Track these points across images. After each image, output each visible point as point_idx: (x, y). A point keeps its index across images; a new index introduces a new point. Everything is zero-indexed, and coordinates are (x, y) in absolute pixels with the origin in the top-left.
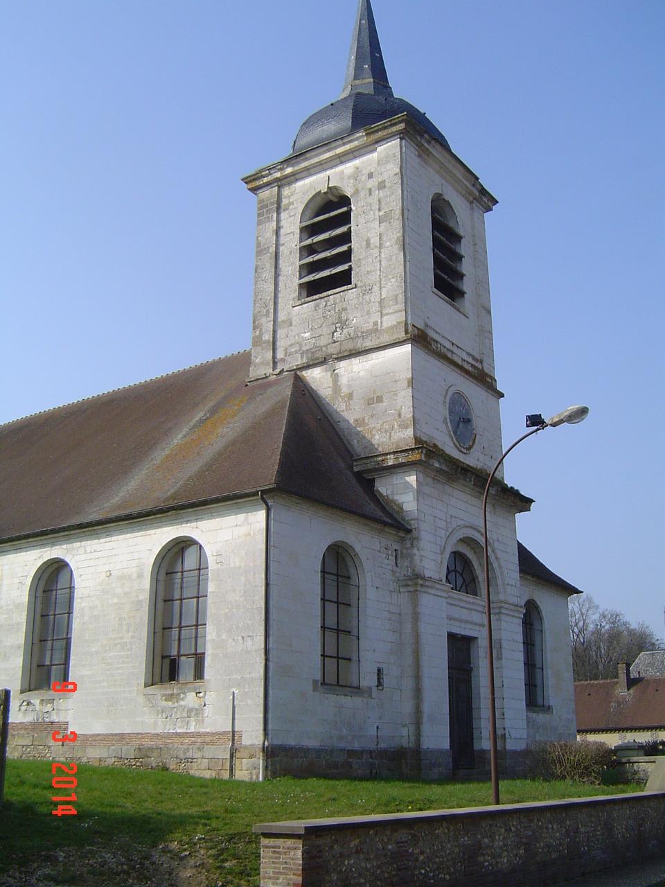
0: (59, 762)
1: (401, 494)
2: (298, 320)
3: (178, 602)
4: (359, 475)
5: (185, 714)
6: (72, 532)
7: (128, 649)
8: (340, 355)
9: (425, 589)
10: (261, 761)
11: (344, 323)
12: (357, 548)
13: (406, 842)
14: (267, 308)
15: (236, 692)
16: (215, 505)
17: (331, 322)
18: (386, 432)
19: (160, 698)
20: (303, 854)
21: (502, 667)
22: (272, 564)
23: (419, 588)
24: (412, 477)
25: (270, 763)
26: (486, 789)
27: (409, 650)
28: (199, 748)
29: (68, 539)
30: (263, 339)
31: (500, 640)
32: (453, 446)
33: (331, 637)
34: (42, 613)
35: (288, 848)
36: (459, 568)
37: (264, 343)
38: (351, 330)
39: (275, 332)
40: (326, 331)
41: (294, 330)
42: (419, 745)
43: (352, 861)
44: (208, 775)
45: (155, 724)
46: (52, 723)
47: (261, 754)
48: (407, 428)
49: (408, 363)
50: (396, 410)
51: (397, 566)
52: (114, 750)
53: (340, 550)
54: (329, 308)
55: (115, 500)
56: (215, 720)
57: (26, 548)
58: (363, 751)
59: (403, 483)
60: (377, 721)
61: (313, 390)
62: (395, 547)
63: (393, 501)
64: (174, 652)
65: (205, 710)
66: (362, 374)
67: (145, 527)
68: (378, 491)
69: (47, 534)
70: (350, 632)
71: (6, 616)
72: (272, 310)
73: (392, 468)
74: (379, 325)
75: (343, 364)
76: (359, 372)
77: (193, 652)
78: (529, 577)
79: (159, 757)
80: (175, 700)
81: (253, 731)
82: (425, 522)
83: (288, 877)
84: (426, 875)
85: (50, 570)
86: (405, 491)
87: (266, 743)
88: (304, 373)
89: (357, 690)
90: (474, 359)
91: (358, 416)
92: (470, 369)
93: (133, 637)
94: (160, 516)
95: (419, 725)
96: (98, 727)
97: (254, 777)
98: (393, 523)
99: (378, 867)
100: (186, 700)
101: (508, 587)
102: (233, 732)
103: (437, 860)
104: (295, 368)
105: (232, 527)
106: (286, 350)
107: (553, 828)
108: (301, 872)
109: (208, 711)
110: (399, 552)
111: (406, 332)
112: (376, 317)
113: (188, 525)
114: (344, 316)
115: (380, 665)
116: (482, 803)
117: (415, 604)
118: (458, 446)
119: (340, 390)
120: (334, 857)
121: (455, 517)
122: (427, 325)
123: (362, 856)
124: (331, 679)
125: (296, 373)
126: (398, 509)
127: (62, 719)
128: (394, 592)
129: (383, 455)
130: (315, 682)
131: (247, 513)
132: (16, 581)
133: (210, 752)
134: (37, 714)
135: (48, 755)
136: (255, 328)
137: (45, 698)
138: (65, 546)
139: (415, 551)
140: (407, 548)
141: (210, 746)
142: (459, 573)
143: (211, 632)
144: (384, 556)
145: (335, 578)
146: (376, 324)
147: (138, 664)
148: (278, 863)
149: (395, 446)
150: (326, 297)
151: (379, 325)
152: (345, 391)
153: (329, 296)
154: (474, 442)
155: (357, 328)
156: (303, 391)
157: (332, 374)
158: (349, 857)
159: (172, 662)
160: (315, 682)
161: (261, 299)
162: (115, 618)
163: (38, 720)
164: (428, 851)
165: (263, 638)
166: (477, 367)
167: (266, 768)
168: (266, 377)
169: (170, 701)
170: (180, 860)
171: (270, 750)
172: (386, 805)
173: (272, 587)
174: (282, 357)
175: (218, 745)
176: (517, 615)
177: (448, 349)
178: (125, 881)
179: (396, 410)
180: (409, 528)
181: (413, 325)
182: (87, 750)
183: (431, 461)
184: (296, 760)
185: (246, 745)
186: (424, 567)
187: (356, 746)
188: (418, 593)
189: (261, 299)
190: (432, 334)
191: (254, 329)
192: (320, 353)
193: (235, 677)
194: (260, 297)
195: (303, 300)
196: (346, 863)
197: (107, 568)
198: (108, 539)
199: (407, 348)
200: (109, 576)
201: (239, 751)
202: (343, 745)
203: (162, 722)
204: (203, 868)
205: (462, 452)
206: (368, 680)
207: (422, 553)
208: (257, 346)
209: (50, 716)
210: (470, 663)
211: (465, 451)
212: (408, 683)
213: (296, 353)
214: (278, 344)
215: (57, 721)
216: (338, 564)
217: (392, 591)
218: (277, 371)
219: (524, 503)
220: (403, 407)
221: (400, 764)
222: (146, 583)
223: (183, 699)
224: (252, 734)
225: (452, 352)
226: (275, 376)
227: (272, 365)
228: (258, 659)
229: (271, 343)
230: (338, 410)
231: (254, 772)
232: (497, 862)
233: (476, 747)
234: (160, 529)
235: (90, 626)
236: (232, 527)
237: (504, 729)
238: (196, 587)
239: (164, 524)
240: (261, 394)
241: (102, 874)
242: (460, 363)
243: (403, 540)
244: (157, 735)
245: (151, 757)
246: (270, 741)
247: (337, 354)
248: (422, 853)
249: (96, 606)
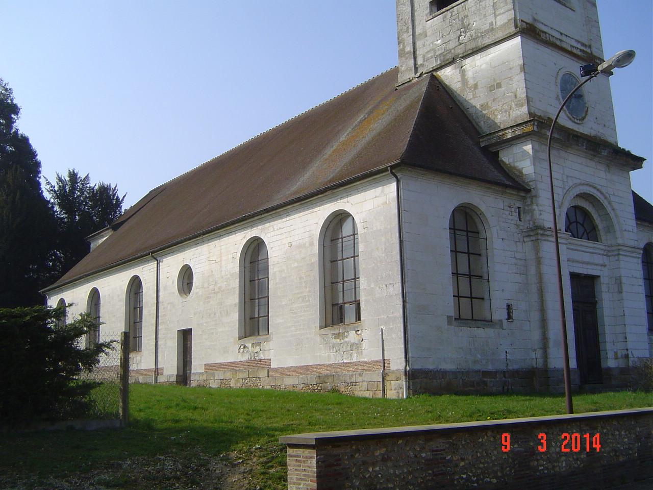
0: (267, 390)
1: (520, 161)
2: (431, 31)
3: (341, 261)
4: (485, 150)
5: (349, 348)
6: (263, 216)
7: (307, 301)
8: (465, 54)
9: (546, 238)
10: (404, 383)
11: (466, 28)
12: (483, 208)
13: (444, 450)
14: (407, 26)
15: (384, 329)
16: (358, 183)
17: (456, 29)
18: (506, 111)
19: (331, 336)
20: (317, 463)
21: (623, 300)
22: (404, 225)
23: (539, 237)
24: (528, 146)
25: (411, 384)
26: (563, 402)
27: (534, 288)
28: (360, 374)
29: (262, 221)
30: (406, 51)
31: (620, 277)
32: (567, 118)
33: (464, 282)
34: (250, 278)
35: (306, 457)
36: (580, 219)
37: (407, 53)
38: (473, 32)
39: (414, 44)
40: (453, 36)
41: (429, 40)
42: (547, 365)
43: (378, 468)
44: (368, 394)
45: (329, 356)
46: (260, 360)
47: (404, 377)
48: (522, 106)
49: (519, 52)
50: (513, 92)
51: (520, 221)
52: (302, 378)
53: (468, 211)
54: (454, 17)
55: (294, 188)
56: (370, 352)
57: (235, 232)
58: (497, 372)
59: (522, 152)
60: (512, 347)
61: (446, 85)
62: (518, 204)
63: (515, 168)
64: (341, 301)
65: (363, 344)
66: (484, 66)
67: (312, 206)
68: (503, 162)
69: (246, 219)
70: (482, 277)
71: (225, 283)
72: (411, 27)
73: (512, 140)
74: (494, 25)
75: (468, 61)
76: (481, 66)
77: (354, 300)
78: (647, 224)
79: (332, 382)
80: (341, 337)
81: (397, 359)
82: (542, 182)
83: (307, 483)
84: (468, 479)
85: (253, 246)
86: (524, 158)
87: (408, 368)
88: (438, 73)
89: (489, 323)
90: (583, 44)
91: (482, 102)
92: (580, 53)
93: (309, 291)
94: (320, 196)
95: (546, 349)
96: (290, 362)
97: (400, 395)
98: (514, 185)
99: (410, 473)
100: (349, 337)
101: (625, 233)
102: (384, 360)
103: (481, 465)
104: (431, 70)
105: (373, 199)
106: (424, 57)
107: (620, 435)
108: (316, 479)
109: (365, 345)
110: (522, 209)
111: (516, 27)
112: (491, 19)
113: (342, 201)
114: (466, 23)
115: (509, 302)
116: (559, 413)
117: (537, 250)
118: (571, 117)
119: (467, 83)
120: (355, 465)
121: (571, 177)
122: (535, 20)
123: (389, 464)
124: (466, 313)
125: (432, 74)
126: (518, 174)
127: (267, 357)
128: (519, 241)
129: (502, 130)
130: (449, 317)
131: (383, 186)
132: (231, 256)
133: (368, 376)
134: (250, 354)
135: (259, 384)
136: (399, 43)
137: (254, 342)
138: (259, 227)
139: (535, 207)
140: (528, 205)
141: (368, 372)
142: (580, 224)
143: (363, 283)
144: (507, 213)
145: (465, 233)
146: (491, 24)
147: (314, 312)
148: (299, 471)
149: (513, 122)
150: (450, 9)
151: (494, 25)
152: (471, 82)
153: (453, 7)
154: (586, 114)
155: (477, 30)
156: (438, 87)
157: (460, 71)
158: (374, 465)
159: (338, 310)
160: (449, 317)
161: (402, 19)
162: (296, 278)
163: (251, 359)
164: (470, 458)
165: (400, 284)
166: (586, 52)
167: (409, 388)
168: (410, 81)
169: (338, 339)
170: (232, 467)
171: (411, 372)
172: (470, 416)
173: (405, 244)
174: (421, 63)
175: (374, 371)
176: (635, 256)
177: (557, 38)
178: (171, 486)
179: (513, 92)
180: (529, 188)
181: (522, 21)
182: (284, 379)
183: (543, 131)
184: (435, 381)
185: (393, 370)
186: (543, 220)
187: (490, 368)
188: (539, 241)
189: (402, 19)
190: (540, 27)
191: (398, 44)
192: (450, 55)
193: (382, 317)
194: (401, 18)
195: (433, 15)
196: (371, 469)
197: (289, 240)
198: (288, 218)
199: (518, 40)
200: (290, 247)
201: (388, 375)
202: (477, 367)
203: (334, 355)
204: (250, 474)
205: (578, 124)
206: (499, 314)
207: (541, 208)
208: (402, 57)
209: (259, 355)
210: (595, 297)
211: (578, 122)
212: (535, 316)
213: (432, 58)
214: (418, 52)
215: (263, 358)
216: (465, 224)
217: (517, 242)
218: (418, 74)
219: (636, 162)
220: (518, 89)
221: (531, 381)
222: (316, 249)
223: (347, 337)
224: (397, 363)
225: (561, 41)
226: (417, 79)
227: (414, 71)
228: (398, 301)
229: (412, 53)
230: (467, 99)
231: (400, 391)
232: (554, 467)
233: (603, 365)
234: (322, 207)
235: (281, 286)
236: (373, 199)
237: (627, 350)
238: (353, 249)
239: (325, 201)
240: (405, 94)
241: (153, 480)
242: (570, 49)
243: (524, 198)
244: (331, 365)
245: (327, 383)
246: (410, 366)
247: (463, 53)
248: (463, 459)
249: (284, 270)
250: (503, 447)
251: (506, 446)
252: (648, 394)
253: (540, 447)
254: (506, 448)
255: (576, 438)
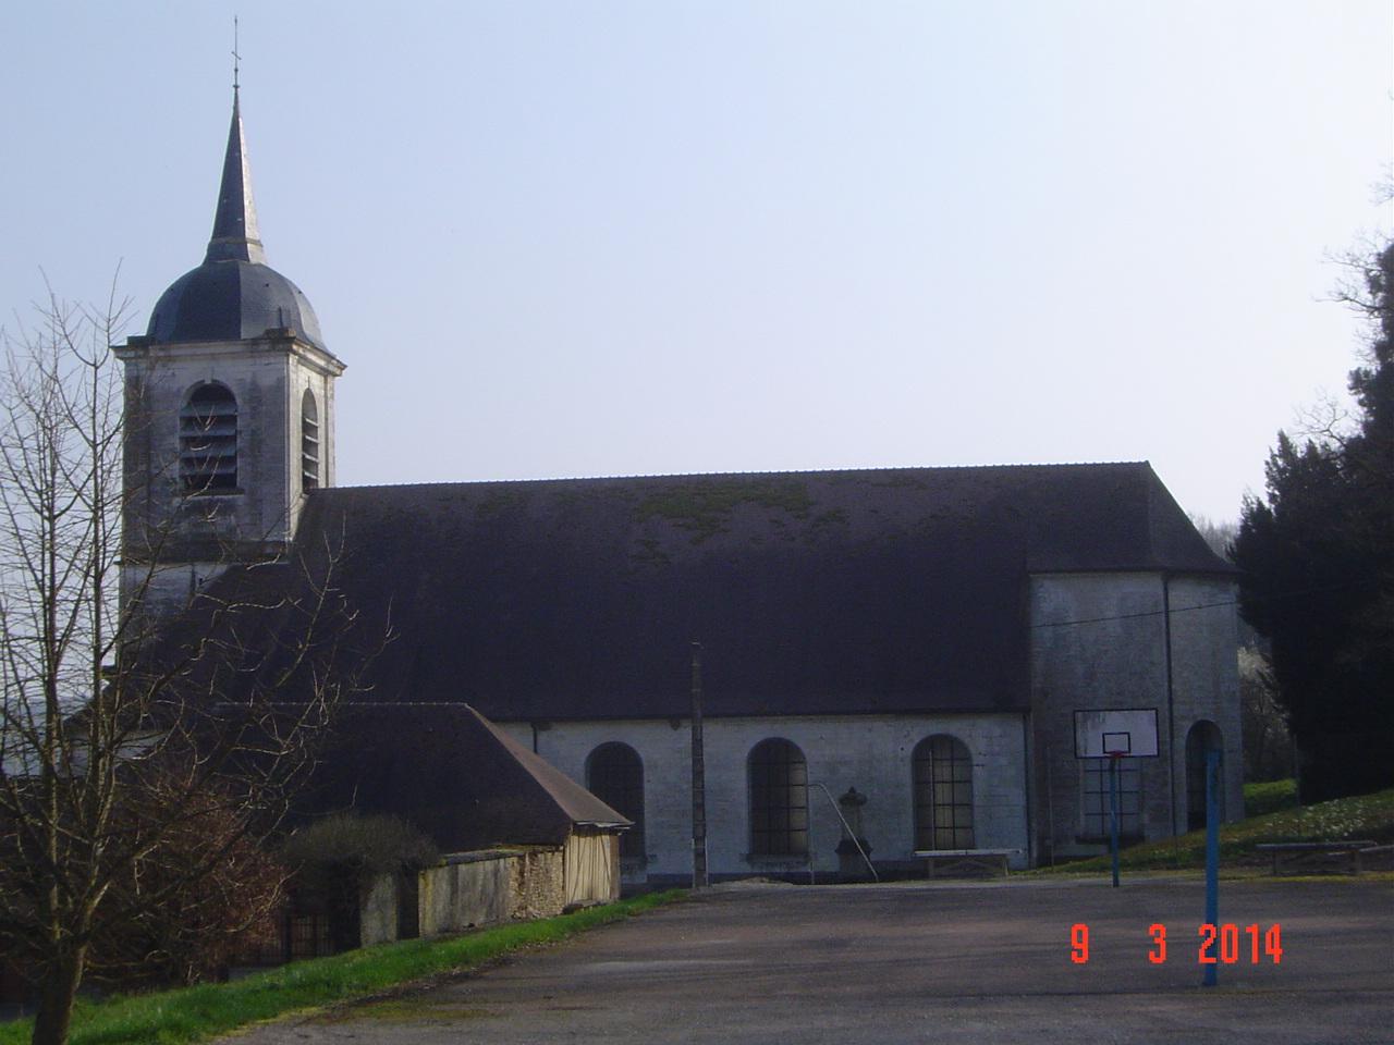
250: (1074, 954)
251: (1080, 952)
252: (106, 1008)
253: (1152, 954)
254: (1080, 956)
255: (1229, 934)
